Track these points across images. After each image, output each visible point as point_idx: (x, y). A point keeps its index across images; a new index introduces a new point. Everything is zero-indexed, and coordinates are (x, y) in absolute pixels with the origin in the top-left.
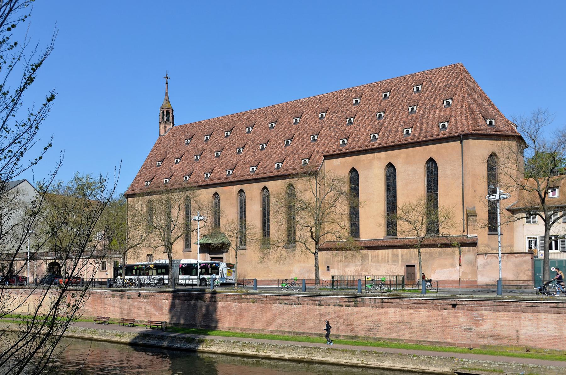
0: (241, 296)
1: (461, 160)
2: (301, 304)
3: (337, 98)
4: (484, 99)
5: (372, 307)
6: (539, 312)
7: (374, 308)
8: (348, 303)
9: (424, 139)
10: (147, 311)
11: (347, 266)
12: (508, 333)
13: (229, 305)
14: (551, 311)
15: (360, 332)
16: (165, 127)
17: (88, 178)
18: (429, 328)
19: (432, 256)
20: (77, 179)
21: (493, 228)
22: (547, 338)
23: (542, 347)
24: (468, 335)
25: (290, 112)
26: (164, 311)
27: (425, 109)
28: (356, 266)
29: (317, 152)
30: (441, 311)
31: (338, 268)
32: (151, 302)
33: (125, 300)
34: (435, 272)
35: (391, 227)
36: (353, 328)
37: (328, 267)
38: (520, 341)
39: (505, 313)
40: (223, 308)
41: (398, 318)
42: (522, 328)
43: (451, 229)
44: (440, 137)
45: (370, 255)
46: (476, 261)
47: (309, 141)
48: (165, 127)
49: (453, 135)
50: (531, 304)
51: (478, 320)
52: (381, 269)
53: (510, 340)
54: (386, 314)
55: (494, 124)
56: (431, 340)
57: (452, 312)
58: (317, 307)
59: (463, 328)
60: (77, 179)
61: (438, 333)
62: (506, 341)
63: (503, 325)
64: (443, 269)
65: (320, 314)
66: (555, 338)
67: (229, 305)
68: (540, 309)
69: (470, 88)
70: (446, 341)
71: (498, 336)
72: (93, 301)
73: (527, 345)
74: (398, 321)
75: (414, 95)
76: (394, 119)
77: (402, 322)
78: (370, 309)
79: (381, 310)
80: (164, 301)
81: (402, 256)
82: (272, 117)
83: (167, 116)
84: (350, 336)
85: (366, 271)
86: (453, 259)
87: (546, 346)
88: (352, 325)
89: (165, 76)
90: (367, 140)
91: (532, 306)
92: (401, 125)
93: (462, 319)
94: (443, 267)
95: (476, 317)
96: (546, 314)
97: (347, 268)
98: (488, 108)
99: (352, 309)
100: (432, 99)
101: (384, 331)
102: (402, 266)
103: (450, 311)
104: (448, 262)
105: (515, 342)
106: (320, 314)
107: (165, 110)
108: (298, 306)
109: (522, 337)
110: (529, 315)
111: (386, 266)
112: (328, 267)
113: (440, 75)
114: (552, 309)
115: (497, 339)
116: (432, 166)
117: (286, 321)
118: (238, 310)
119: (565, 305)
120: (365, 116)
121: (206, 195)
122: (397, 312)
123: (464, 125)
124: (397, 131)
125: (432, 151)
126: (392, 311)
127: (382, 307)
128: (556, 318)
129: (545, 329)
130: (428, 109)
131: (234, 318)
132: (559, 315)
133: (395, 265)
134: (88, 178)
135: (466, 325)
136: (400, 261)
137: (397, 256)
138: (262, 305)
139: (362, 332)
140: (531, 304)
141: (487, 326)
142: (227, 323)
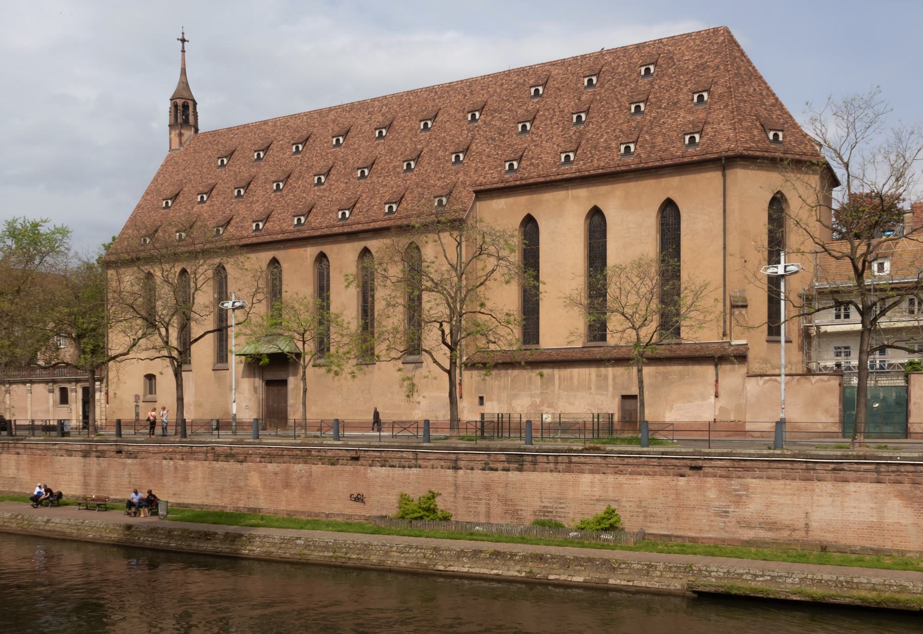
0: (309, 451)
1: (722, 204)
2: (420, 467)
3: (502, 85)
4: (764, 93)
5: (551, 471)
6: (846, 481)
7: (555, 474)
8: (506, 465)
9: (658, 164)
10: (133, 480)
11: (515, 396)
14: (867, 478)
16: (181, 135)
18: (653, 511)
24: (719, 522)
25: (414, 109)
27: (660, 108)
29: (463, 183)
30: (675, 478)
31: (499, 401)
34: (672, 408)
37: (481, 398)
38: (810, 533)
39: (788, 482)
40: (276, 474)
41: (597, 492)
44: (686, 160)
45: (557, 377)
48: (181, 135)
50: (832, 466)
53: (795, 530)
55: (781, 139)
56: (655, 532)
58: (450, 472)
59: (712, 510)
62: (785, 534)
63: (782, 504)
65: (456, 486)
75: (642, 82)
76: (603, 125)
78: (548, 476)
79: (568, 476)
80: (165, 462)
81: (614, 378)
83: (183, 111)
89: (180, 37)
90: (555, 163)
91: (834, 469)
92: (617, 138)
95: (736, 490)
96: (858, 484)
97: (517, 398)
98: (771, 110)
99: (514, 476)
100: (672, 91)
102: (613, 396)
103: (690, 478)
105: (803, 534)
106: (456, 486)
107: (180, 102)
108: (414, 470)
109: (814, 525)
110: (828, 486)
111: (586, 397)
112: (481, 398)
113: (688, 47)
114: (869, 475)
115: (770, 530)
118: (304, 479)
119: (922, 468)
120: (552, 118)
122: (596, 480)
123: (728, 140)
124: (608, 148)
126: (586, 478)
127: (568, 470)
129: (855, 510)
130: (665, 108)
132: (879, 485)
136: (611, 389)
137: (606, 378)
138: (349, 468)
141: (753, 507)
142: (284, 503)
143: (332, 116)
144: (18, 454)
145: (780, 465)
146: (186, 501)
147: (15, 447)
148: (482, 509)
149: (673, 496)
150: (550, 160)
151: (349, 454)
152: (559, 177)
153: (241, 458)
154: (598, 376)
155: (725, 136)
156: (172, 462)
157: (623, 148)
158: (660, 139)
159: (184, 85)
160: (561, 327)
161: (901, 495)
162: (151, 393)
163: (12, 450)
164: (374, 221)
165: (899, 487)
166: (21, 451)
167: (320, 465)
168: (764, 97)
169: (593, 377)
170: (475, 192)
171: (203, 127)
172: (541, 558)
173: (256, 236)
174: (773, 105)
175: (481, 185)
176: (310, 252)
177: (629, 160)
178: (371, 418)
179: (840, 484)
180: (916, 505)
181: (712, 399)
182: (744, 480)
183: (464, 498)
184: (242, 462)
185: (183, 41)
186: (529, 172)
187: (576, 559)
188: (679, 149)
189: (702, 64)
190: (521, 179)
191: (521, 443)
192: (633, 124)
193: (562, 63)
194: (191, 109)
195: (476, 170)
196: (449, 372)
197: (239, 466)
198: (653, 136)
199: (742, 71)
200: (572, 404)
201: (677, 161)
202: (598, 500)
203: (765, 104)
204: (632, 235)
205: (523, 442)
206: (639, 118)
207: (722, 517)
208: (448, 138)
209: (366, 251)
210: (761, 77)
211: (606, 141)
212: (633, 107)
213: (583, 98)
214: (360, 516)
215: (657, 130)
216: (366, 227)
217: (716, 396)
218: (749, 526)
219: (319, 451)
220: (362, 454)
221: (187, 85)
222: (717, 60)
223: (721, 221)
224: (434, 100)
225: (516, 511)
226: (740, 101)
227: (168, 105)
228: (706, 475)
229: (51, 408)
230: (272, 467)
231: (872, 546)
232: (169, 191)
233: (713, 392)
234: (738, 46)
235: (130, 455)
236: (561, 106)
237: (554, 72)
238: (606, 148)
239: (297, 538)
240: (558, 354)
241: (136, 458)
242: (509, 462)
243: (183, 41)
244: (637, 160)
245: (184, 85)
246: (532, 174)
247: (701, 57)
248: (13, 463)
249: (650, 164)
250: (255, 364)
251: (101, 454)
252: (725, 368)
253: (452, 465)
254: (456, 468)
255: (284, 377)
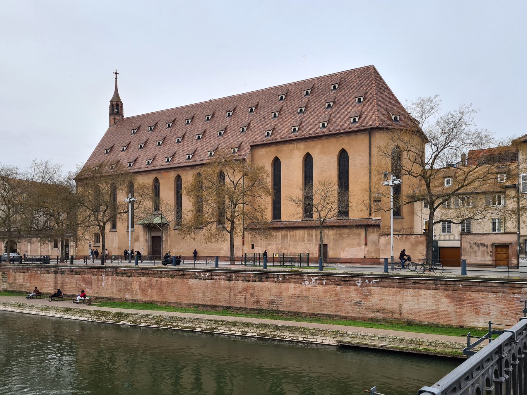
0: (161, 271)
1: (368, 151)
2: (213, 279)
3: (265, 95)
4: (391, 97)
5: (275, 282)
7: (277, 283)
8: (254, 279)
9: (338, 132)
10: (78, 285)
11: (269, 244)
12: (392, 307)
13: (151, 281)
14: (430, 287)
15: (265, 306)
17: (46, 163)
18: (324, 302)
19: (341, 236)
20: (35, 165)
21: (397, 213)
22: (426, 312)
23: (421, 320)
24: (357, 308)
25: (224, 106)
26: (93, 286)
27: (340, 105)
28: (277, 244)
29: (246, 141)
30: (335, 286)
31: (261, 247)
32: (82, 278)
33: (59, 276)
34: (344, 251)
35: (308, 210)
36: (259, 301)
38: (402, 315)
39: (391, 289)
40: (145, 282)
41: (298, 293)
42: (404, 303)
43: (357, 212)
44: (351, 130)
45: (289, 235)
46: (379, 241)
47: (239, 133)
48: (115, 119)
49: (362, 128)
50: (413, 281)
51: (367, 295)
52: (298, 247)
53: (394, 313)
54: (287, 289)
55: (398, 119)
56: (326, 313)
57: (344, 288)
58: (227, 282)
59: (353, 302)
60: (35, 165)
61: (332, 307)
62: (390, 315)
63: (388, 300)
64: (349, 248)
65: (230, 288)
66: (432, 312)
67: (151, 281)
68: (420, 285)
69: (380, 87)
70: (337, 314)
71: (384, 309)
72: (30, 277)
73: (409, 318)
74: (297, 295)
75: (332, 93)
76: (313, 114)
77: (301, 296)
78: (274, 284)
79: (283, 285)
80: (93, 277)
82: (209, 111)
83: (116, 107)
84: (255, 309)
85: (285, 249)
86: (360, 239)
87: (425, 320)
88: (258, 299)
90: (289, 132)
91: (414, 283)
92: (319, 120)
93: (353, 294)
94: (352, 246)
96: (426, 290)
97: (273, 246)
98: (394, 106)
99: (258, 284)
100: (346, 97)
101: (285, 304)
102: (316, 245)
103: (343, 286)
104: (356, 241)
105: (398, 315)
106: (230, 288)
107: (115, 103)
108: (210, 281)
109: (404, 311)
110: (411, 291)
111: (305, 244)
113: (354, 76)
114: (431, 286)
115: (382, 313)
116: (343, 158)
117: (201, 295)
118: (158, 285)
120: (288, 110)
121: (147, 181)
123: (372, 120)
124: (314, 125)
125: (344, 143)
126: (292, 286)
127: (284, 282)
128: (434, 293)
130: (342, 105)
131: (155, 291)
132: (436, 291)
133: (310, 244)
134: (46, 163)
135: (356, 299)
136: (314, 241)
137: (312, 236)
138: (180, 280)
139: (266, 305)
140: (413, 281)
141: (374, 301)
142: (149, 297)
143: (186, 110)
144: (24, 272)
145: (387, 280)
146: (103, 296)
147: (23, 269)
148: (243, 300)
149: (334, 295)
150: (287, 131)
151: (180, 273)
152: (290, 139)
153: (129, 275)
154: (309, 235)
155: (372, 118)
156: (96, 277)
157: (321, 124)
158: (339, 120)
159: (116, 94)
160: (291, 212)
161: (448, 296)
162: (97, 242)
163: (22, 271)
164: (203, 160)
165: (447, 292)
166: (25, 271)
167: (166, 278)
168: (391, 99)
169: (306, 235)
170: (251, 146)
171: (126, 115)
172: (265, 326)
173: (167, 165)
174: (395, 103)
175: (254, 142)
176: (173, 175)
177: (324, 130)
178: (192, 255)
179: (417, 290)
180: (455, 302)
181: (364, 246)
182: (369, 288)
183: (234, 295)
184: (129, 277)
185: (116, 73)
186: (276, 136)
187: (283, 326)
188: (348, 125)
189: (361, 84)
190: (273, 140)
191: (261, 268)
192: (327, 113)
193: (295, 84)
194: (120, 107)
195: (252, 135)
196: (230, 233)
197: (128, 278)
198: (336, 118)
199: (380, 87)
200: (296, 248)
201: (346, 130)
202: (298, 297)
203: (391, 103)
204: (326, 167)
205: (262, 268)
206: (329, 110)
207: (358, 306)
208: (239, 120)
209: (199, 174)
210: (389, 90)
211: (313, 121)
212: (327, 104)
213: (303, 101)
214: (185, 304)
215: (338, 115)
216: (199, 163)
217: (366, 245)
218: (372, 311)
219: (166, 271)
220: (186, 273)
221: (118, 95)
222: (368, 82)
223: (368, 160)
224: (234, 102)
225: (259, 301)
226: (378, 101)
227: (109, 104)
228: (350, 285)
229: (50, 250)
230: (143, 279)
231: (434, 323)
232: (109, 146)
233: (363, 242)
234: (379, 75)
235: (77, 273)
236: (293, 104)
237: (290, 89)
238: (313, 125)
239: (150, 315)
240: (289, 224)
241: (79, 274)
242: (255, 277)
243: (116, 73)
244: (328, 130)
245: (116, 94)
246: (277, 137)
247: (360, 80)
248: (22, 277)
249: (334, 132)
250: (149, 227)
251: (63, 273)
252: (371, 230)
253: (229, 278)
254: (230, 280)
255: (160, 234)
